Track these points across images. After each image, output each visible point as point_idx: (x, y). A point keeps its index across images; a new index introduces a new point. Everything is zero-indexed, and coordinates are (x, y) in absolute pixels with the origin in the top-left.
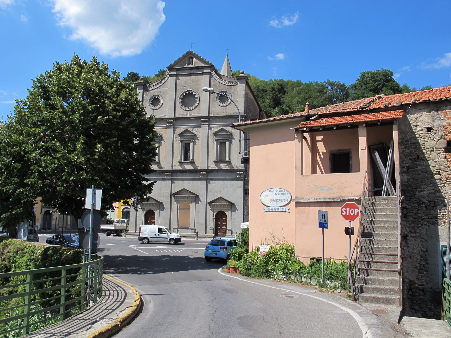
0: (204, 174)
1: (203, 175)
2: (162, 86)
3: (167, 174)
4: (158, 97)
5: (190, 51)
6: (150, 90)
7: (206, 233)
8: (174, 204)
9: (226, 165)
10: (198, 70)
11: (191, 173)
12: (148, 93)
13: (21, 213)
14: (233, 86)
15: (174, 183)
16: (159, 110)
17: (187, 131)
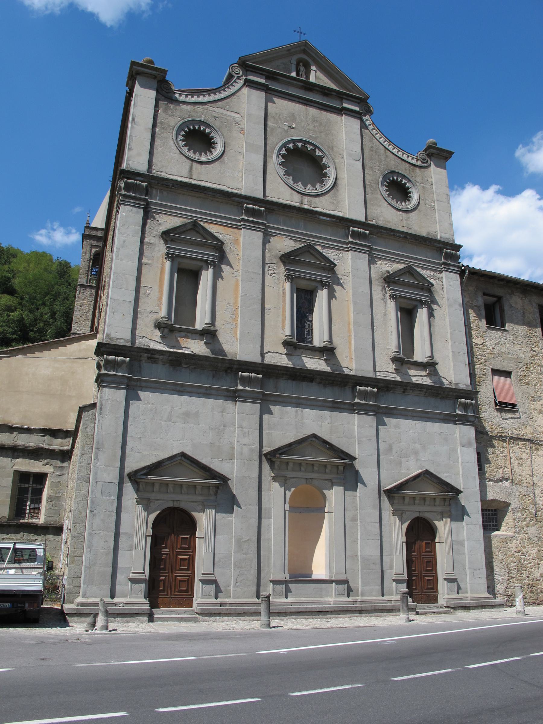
0: (372, 392)
1: (364, 395)
2: (219, 103)
3: (249, 378)
5: (306, 44)
6: (180, 102)
7: (112, 596)
8: (269, 490)
9: (424, 373)
10: (325, 98)
11: (325, 386)
12: (172, 106)
13: (95, 286)
14: (420, 167)
15: (270, 412)
16: (210, 166)
17: (309, 249)
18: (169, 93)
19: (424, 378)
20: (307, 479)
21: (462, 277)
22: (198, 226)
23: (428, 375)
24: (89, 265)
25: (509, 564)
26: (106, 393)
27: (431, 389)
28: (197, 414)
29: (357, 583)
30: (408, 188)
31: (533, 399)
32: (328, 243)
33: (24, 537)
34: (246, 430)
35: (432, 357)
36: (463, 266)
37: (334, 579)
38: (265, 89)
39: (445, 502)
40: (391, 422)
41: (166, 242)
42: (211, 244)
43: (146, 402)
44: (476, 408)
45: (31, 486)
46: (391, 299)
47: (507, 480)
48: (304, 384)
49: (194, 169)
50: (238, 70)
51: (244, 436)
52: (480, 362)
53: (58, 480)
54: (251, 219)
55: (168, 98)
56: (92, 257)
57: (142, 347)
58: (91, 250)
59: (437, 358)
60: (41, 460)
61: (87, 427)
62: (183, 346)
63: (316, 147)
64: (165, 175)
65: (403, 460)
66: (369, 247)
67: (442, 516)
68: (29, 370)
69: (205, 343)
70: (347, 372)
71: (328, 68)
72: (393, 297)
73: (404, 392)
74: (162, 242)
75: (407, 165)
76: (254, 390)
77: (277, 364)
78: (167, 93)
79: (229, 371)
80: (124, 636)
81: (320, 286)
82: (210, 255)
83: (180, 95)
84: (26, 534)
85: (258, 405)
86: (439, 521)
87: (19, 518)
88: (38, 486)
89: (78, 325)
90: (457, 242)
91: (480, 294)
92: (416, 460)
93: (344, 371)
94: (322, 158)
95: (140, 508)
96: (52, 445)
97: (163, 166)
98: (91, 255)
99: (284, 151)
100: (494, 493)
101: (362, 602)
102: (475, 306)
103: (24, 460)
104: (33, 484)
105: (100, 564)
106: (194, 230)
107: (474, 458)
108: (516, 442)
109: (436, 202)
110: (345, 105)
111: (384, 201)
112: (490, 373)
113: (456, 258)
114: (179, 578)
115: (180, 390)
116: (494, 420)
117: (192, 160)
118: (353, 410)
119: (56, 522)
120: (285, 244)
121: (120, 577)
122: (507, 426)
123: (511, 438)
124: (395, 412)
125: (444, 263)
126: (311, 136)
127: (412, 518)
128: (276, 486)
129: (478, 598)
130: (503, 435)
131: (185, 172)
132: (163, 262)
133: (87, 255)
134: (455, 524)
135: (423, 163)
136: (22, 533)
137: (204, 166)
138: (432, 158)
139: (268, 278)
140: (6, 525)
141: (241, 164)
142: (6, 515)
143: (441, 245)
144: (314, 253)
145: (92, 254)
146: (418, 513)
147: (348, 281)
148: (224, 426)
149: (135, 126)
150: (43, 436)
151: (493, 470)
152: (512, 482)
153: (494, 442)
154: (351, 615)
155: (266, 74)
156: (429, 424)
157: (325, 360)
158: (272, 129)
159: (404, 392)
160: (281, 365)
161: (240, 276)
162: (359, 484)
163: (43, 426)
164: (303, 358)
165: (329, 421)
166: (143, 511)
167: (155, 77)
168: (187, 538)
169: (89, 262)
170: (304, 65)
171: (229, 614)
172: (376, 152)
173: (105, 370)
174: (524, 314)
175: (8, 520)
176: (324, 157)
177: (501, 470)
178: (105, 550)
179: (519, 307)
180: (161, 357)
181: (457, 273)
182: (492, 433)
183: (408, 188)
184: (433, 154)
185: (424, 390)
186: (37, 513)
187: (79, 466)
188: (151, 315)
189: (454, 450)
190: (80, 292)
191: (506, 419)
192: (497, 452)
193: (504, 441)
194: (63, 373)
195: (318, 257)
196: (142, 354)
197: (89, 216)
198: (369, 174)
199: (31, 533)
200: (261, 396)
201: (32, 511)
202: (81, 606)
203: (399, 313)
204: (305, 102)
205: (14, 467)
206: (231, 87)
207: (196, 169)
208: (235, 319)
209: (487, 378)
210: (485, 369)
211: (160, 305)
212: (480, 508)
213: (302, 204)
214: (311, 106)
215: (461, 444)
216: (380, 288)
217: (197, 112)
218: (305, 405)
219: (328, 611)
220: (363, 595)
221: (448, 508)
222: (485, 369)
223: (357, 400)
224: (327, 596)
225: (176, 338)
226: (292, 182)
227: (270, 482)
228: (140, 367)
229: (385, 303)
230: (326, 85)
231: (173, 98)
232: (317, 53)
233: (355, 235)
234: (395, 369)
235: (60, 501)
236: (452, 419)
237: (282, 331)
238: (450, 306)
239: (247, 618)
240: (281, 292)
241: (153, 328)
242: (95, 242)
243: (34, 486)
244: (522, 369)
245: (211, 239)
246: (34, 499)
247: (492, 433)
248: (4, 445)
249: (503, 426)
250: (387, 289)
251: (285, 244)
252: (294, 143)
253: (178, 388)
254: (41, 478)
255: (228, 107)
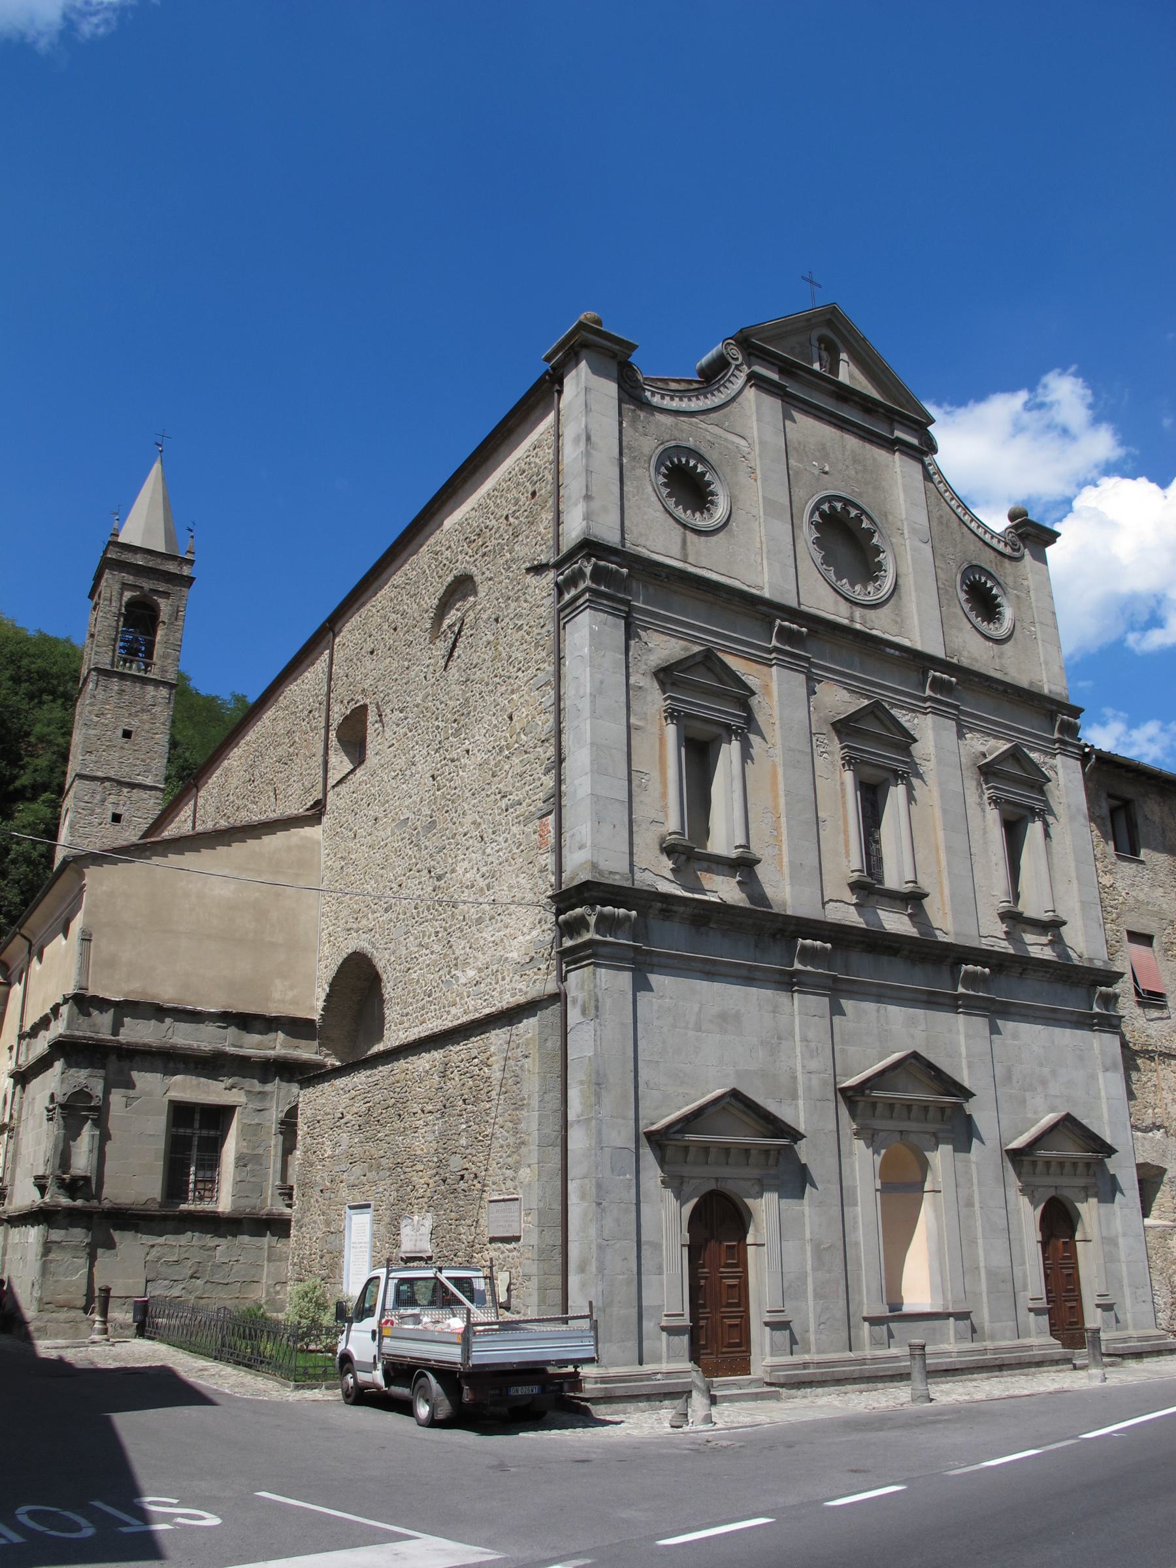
3: (814, 949)
4: (700, 469)
5: (833, 310)
8: (851, 1153)
9: (1044, 940)
12: (642, 415)
14: (1010, 558)
18: (635, 388)
19: (1045, 948)
20: (901, 1132)
21: (1084, 766)
22: (714, 658)
23: (1051, 943)
24: (117, 628)
25: (1171, 1276)
26: (603, 977)
27: (1060, 969)
28: (737, 1016)
29: (984, 1316)
30: (996, 597)
32: (898, 697)
33: (194, 1243)
34: (813, 1045)
35: (747, 846)
36: (1086, 746)
37: (951, 1310)
38: (782, 393)
39: (1088, 1171)
40: (1008, 1026)
41: (663, 688)
42: (733, 694)
43: (661, 994)
44: (1110, 1000)
45: (197, 1132)
46: (992, 804)
47: (1159, 1128)
48: (885, 959)
49: (689, 544)
50: (736, 353)
51: (812, 1057)
52: (1111, 918)
53: (257, 1121)
54: (787, 648)
55: (635, 399)
56: (123, 609)
57: (645, 888)
58: (121, 595)
59: (756, 849)
60: (221, 1078)
61: (546, 1040)
62: (706, 887)
63: (863, 512)
64: (645, 553)
65: (1028, 1095)
66: (956, 707)
67: (1086, 1193)
68: (190, 886)
69: (739, 882)
70: (942, 937)
71: (867, 358)
72: (995, 801)
73: (1021, 974)
74: (656, 685)
75: (992, 554)
76: (820, 971)
77: (843, 922)
78: (632, 387)
79: (778, 936)
80: (743, 1433)
81: (892, 780)
82: (727, 713)
83: (653, 394)
84: (196, 1234)
85: (827, 999)
86: (1082, 1202)
87: (179, 1201)
88: (212, 1133)
89: (93, 758)
91: (1104, 795)
92: (1046, 1096)
93: (936, 936)
94: (870, 534)
95: (669, 1194)
96: (241, 1047)
97: (641, 535)
98: (121, 605)
99: (817, 518)
100: (1144, 1151)
101: (996, 1350)
102: (1098, 817)
103: (189, 1077)
104: (201, 1128)
105: (620, 1302)
106: (704, 664)
108: (1167, 1062)
109: (1037, 625)
110: (898, 434)
111: (966, 620)
112: (1126, 938)
113: (1071, 730)
114: (728, 1321)
115: (710, 972)
116: (1135, 1023)
117: (685, 526)
118: (788, 984)
119: (255, 1208)
120: (837, 698)
121: (649, 1325)
122: (1154, 1034)
123: (1161, 1054)
124: (1013, 1010)
125: (1059, 741)
126: (853, 491)
127: (1047, 1197)
128: (859, 1145)
129: (1147, 1338)
130: (1150, 1048)
131: (676, 550)
132: (661, 724)
133: (114, 604)
134: (1105, 1207)
135: (1014, 550)
136: (189, 1233)
137: (703, 538)
138: (1027, 542)
139: (819, 761)
140: (158, 1216)
141: (758, 539)
142: (156, 1196)
143: (1054, 708)
144: (882, 717)
145: (123, 604)
146: (1053, 1189)
147: (928, 768)
148: (779, 1038)
149: (592, 451)
150: (224, 1028)
151: (1139, 1110)
152: (1166, 1132)
153: (1139, 1061)
154: (988, 1374)
155: (780, 364)
156: (1057, 1031)
157: (910, 916)
158: (797, 473)
159: (1021, 974)
160: (850, 924)
161: (778, 754)
162: (975, 1141)
163: (223, 1007)
164: (878, 911)
165: (923, 1027)
166: (673, 1200)
167: (614, 356)
168: (734, 1246)
169: (118, 621)
171: (824, 1381)
172: (947, 526)
173: (598, 932)
174: (1163, 832)
175: (160, 1206)
176: (875, 532)
177: (1150, 1111)
178: (626, 1276)
179: (1157, 819)
180: (682, 909)
181: (1077, 759)
182: (1135, 1044)
183: (996, 597)
184: (1030, 535)
185: (1051, 970)
186: (209, 1190)
187: (540, 1116)
188: (654, 827)
189: (1093, 1077)
190: (97, 684)
191: (1152, 1020)
192: (1144, 1079)
193: (1152, 1059)
194: (257, 894)
195: (888, 723)
196: (653, 903)
197: (192, 537)
198: (942, 569)
199: (207, 1233)
200: (830, 982)
201: (200, 1186)
202: (602, 1382)
203: (683, 750)
204: (839, 423)
205: (168, 1094)
206: (727, 384)
207: (692, 543)
208: (777, 838)
209: (1121, 946)
210: (1118, 931)
211: (664, 808)
212: (1136, 1179)
213: (852, 621)
214: (849, 431)
215: (1104, 1066)
216: (974, 783)
217: (682, 431)
218: (889, 998)
219: (957, 1369)
220: (992, 1338)
221: (1093, 1181)
222: (1118, 931)
223: (961, 990)
224: (942, 1343)
225: (695, 872)
226: (834, 579)
227: (851, 1140)
228: (646, 927)
229: (983, 811)
230: (865, 392)
231: (644, 401)
232: (852, 330)
233: (938, 685)
234: (1006, 933)
235: (261, 1165)
236: (1088, 1021)
237: (845, 862)
238: (1072, 818)
239: (849, 1387)
240: (838, 787)
241: (658, 852)
242: (131, 577)
243: (204, 1133)
244: (1167, 931)
245: (733, 685)
246: (204, 1160)
247: (1135, 1044)
248: (151, 1047)
249: (1149, 1032)
250: (984, 786)
251: (837, 698)
252: (845, 504)
253: (708, 968)
254: (219, 1117)
255: (727, 424)
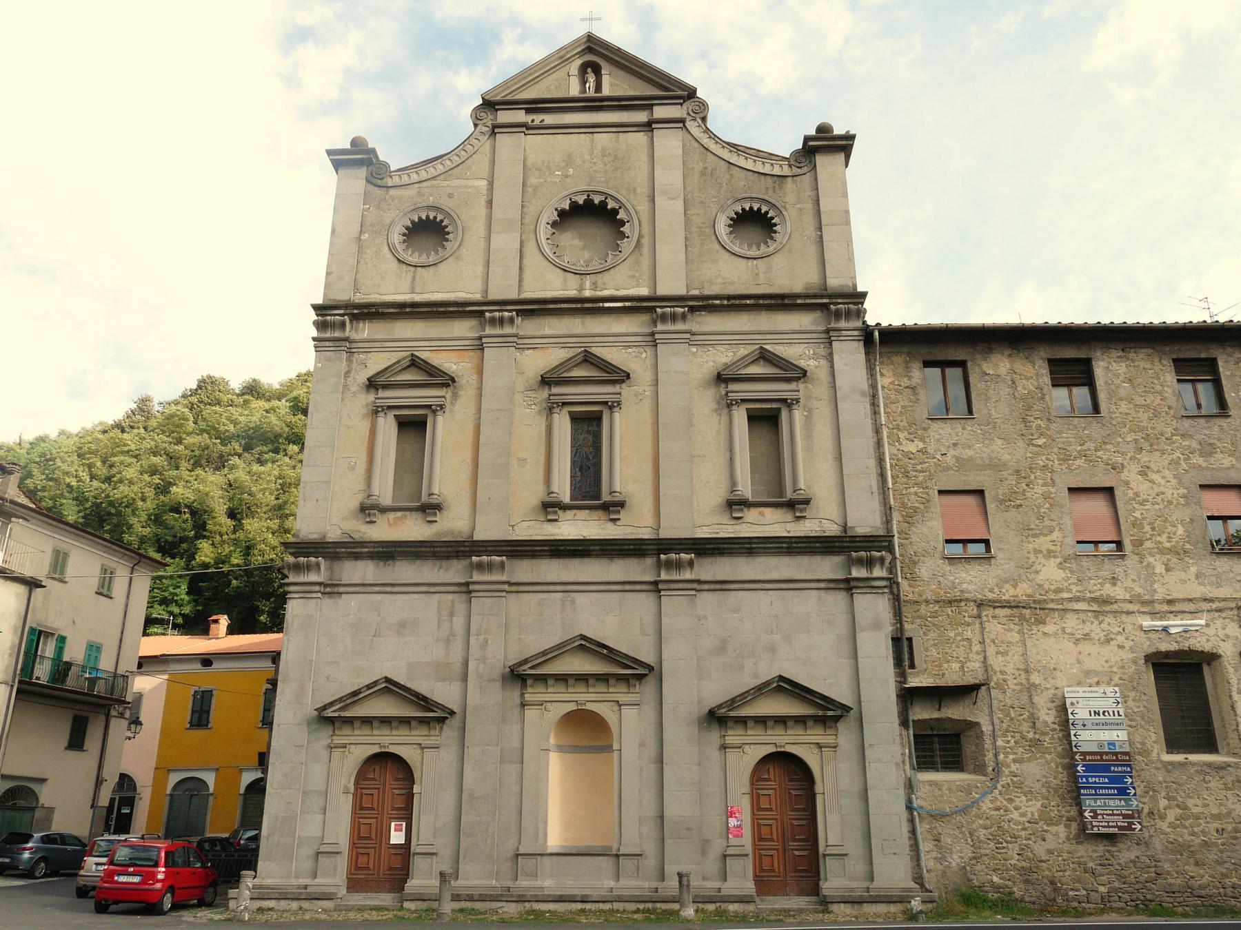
7: (315, 876)
31: (1030, 532)
63: (607, 195)
78: (380, 179)
90: (860, 289)
107: (887, 648)
170: (593, 71)
181: (859, 340)
